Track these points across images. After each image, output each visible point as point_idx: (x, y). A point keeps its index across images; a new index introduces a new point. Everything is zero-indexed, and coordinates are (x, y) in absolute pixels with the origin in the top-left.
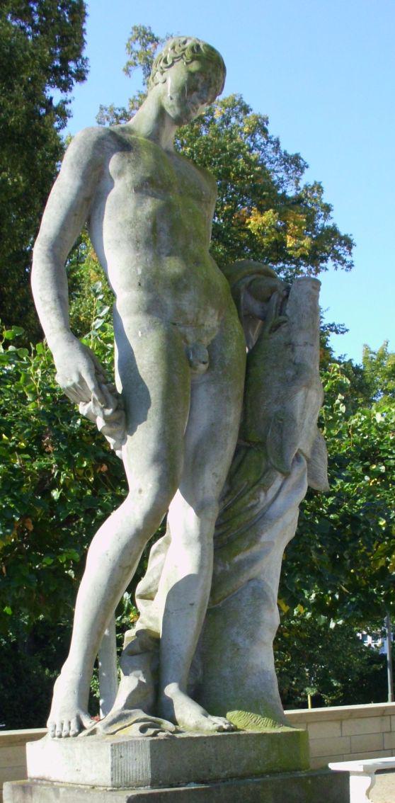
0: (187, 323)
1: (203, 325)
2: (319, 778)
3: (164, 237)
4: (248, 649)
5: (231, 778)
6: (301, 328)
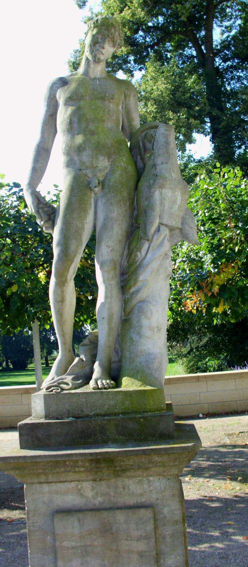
0: (87, 168)
1: (98, 166)
2: (149, 418)
3: (75, 125)
4: (138, 341)
5: (98, 416)
6: (159, 155)
